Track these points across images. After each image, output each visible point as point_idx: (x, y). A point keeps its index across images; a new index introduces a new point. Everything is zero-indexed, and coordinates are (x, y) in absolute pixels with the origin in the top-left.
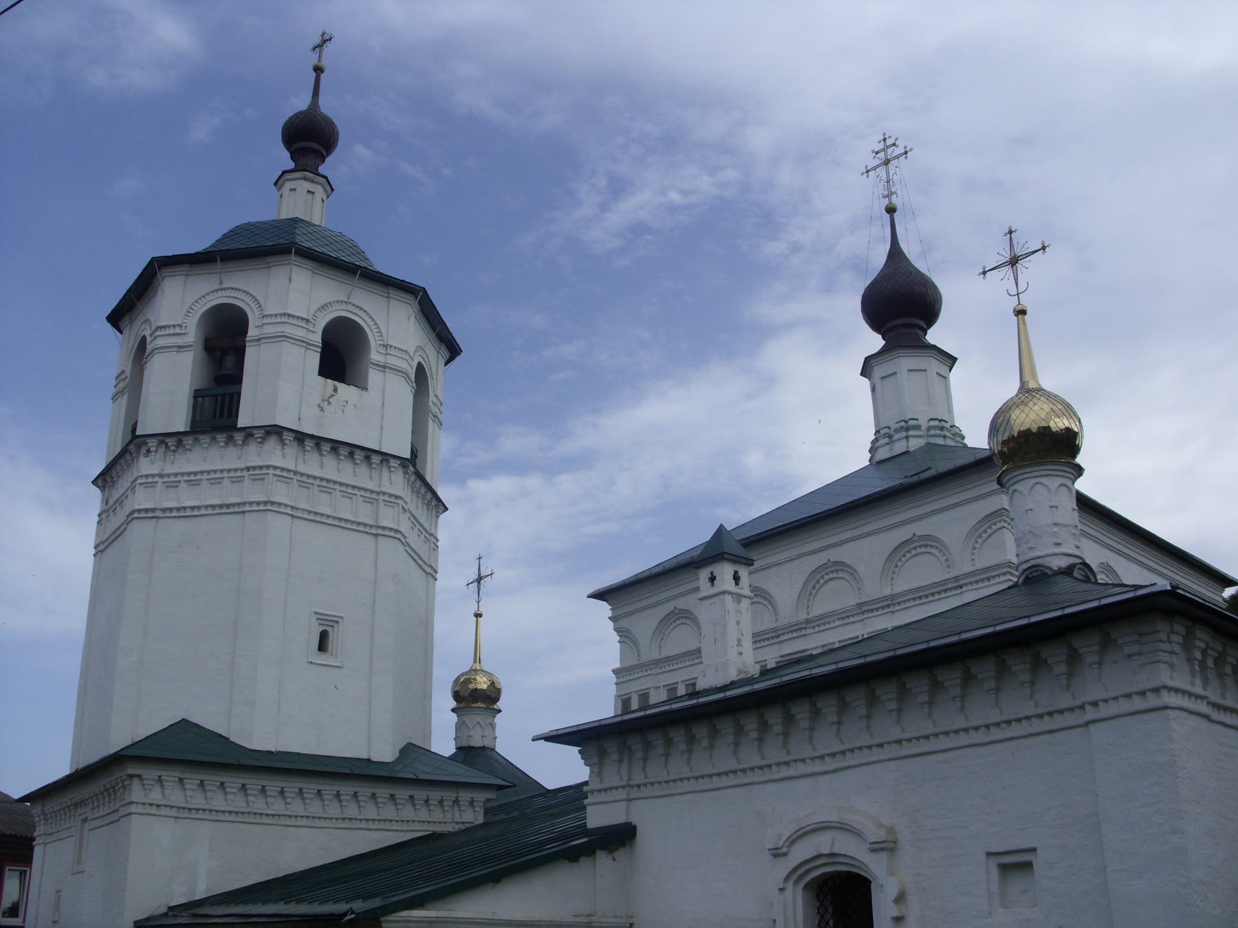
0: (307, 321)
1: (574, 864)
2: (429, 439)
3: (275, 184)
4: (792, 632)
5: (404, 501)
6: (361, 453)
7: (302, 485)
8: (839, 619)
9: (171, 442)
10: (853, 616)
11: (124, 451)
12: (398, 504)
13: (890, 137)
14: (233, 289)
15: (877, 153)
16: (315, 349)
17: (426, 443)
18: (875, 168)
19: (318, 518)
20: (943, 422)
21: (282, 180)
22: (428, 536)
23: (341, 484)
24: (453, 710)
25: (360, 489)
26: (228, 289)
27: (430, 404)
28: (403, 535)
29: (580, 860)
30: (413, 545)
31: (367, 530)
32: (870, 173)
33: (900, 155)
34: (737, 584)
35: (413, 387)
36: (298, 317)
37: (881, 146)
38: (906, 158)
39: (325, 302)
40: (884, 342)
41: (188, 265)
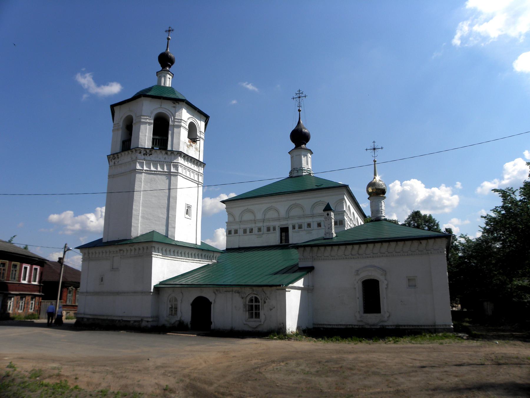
7: (193, 173)
9: (199, 163)
13: (301, 91)
14: (164, 108)
15: (297, 94)
18: (296, 98)
19: (187, 178)
33: (304, 96)
37: (298, 92)
38: (305, 98)
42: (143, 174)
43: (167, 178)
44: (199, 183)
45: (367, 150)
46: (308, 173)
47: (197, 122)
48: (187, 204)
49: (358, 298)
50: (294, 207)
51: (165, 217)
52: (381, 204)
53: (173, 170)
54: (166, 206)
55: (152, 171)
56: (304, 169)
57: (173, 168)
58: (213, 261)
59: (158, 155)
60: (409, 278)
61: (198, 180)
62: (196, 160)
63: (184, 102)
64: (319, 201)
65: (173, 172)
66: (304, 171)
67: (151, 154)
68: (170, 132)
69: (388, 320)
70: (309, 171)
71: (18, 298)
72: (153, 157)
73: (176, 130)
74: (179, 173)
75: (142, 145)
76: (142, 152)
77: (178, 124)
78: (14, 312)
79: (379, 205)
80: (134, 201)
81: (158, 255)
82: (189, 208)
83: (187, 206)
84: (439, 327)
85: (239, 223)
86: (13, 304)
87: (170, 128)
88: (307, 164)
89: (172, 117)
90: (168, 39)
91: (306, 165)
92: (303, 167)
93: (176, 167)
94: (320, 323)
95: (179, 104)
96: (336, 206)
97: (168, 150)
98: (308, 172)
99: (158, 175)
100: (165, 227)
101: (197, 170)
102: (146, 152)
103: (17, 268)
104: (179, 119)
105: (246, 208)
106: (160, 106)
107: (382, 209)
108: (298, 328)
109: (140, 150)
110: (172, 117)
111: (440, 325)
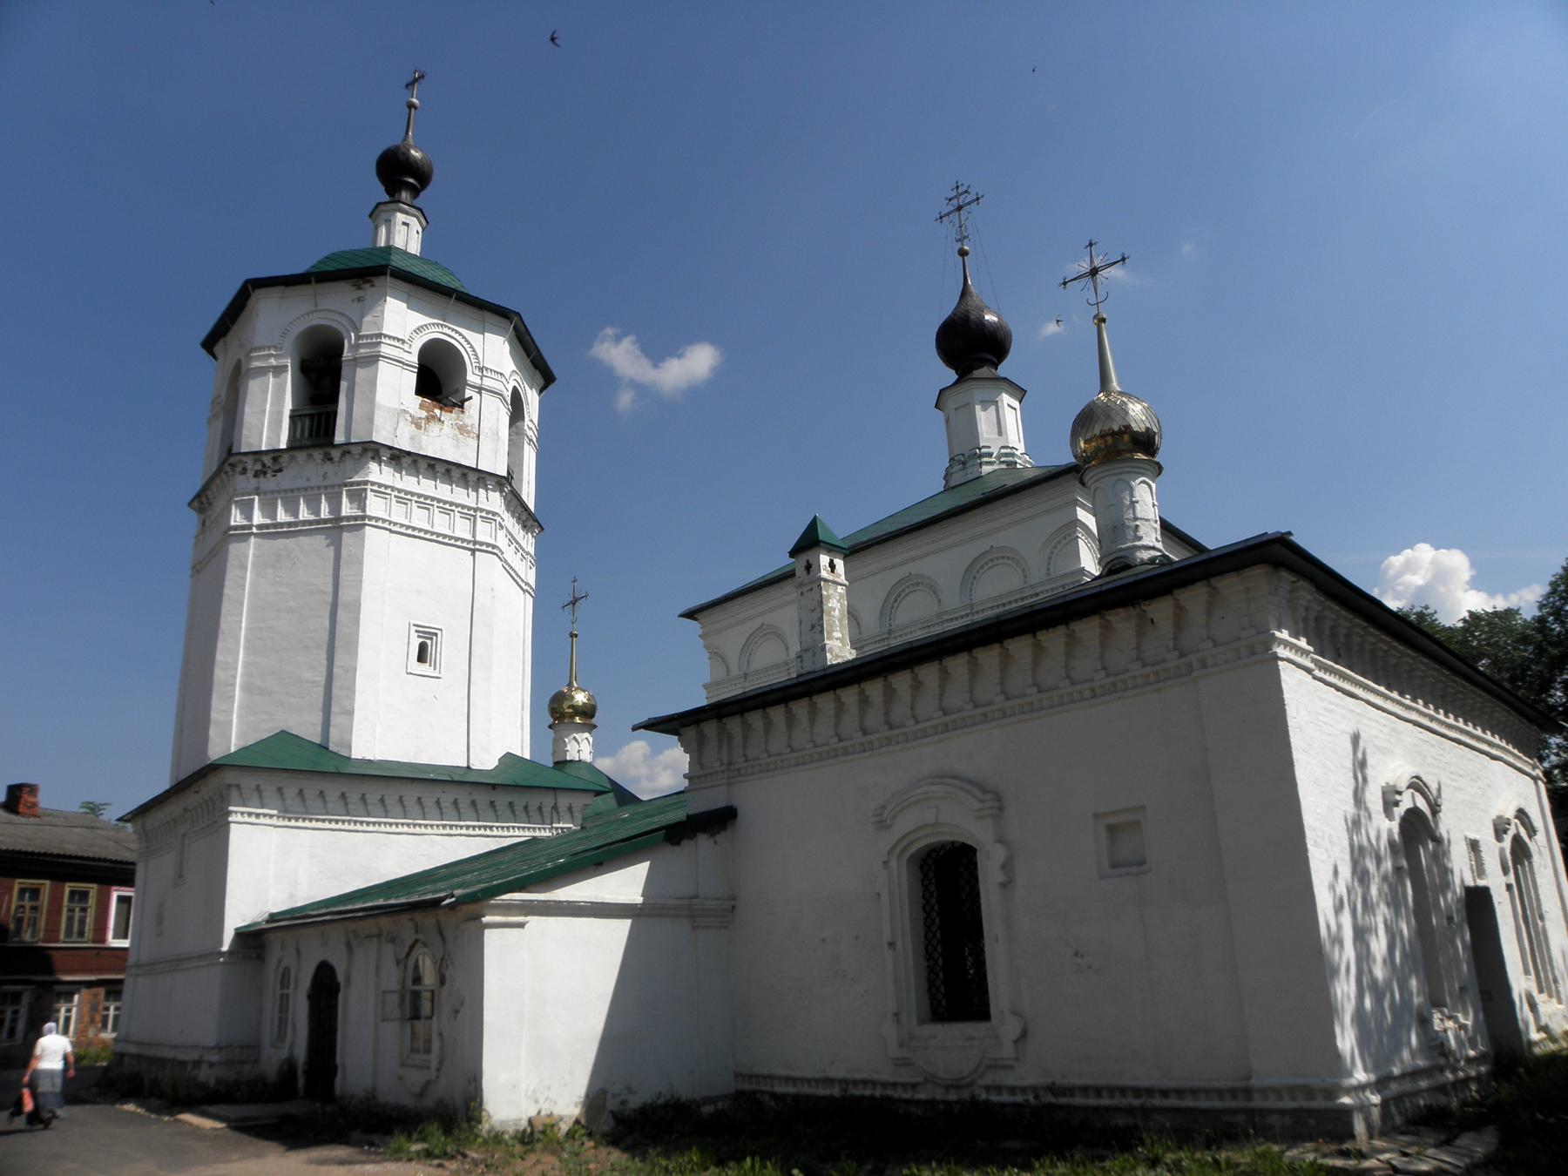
0: (403, 342)
1: (676, 847)
2: (524, 468)
3: (370, 216)
4: (875, 642)
5: (502, 518)
6: (457, 471)
7: (400, 500)
8: (920, 629)
10: (933, 625)
11: (220, 470)
12: (495, 520)
13: (962, 185)
14: (328, 310)
15: (950, 200)
16: (413, 369)
17: (522, 465)
18: (948, 214)
19: (416, 533)
20: (1014, 450)
21: (376, 212)
22: (525, 555)
23: (439, 501)
24: (550, 727)
25: (457, 505)
26: (324, 310)
27: (526, 428)
28: (501, 551)
29: (682, 843)
30: (510, 562)
31: (465, 545)
32: (944, 219)
34: (833, 571)
35: (509, 409)
36: (394, 338)
37: (954, 193)
39: (417, 325)
40: (957, 377)
41: (282, 287)
42: (252, 539)
43: (328, 541)
44: (477, 547)
45: (1065, 283)
46: (1003, 462)
47: (464, 337)
48: (414, 625)
49: (892, 945)
50: (907, 591)
51: (321, 678)
52: (1132, 495)
53: (347, 509)
54: (325, 637)
55: (282, 525)
56: (983, 450)
57: (351, 503)
58: (554, 825)
59: (309, 468)
60: (1112, 820)
61: (474, 536)
62: (454, 468)
63: (385, 274)
64: (988, 548)
65: (348, 518)
66: (985, 459)
67: (280, 470)
68: (344, 385)
69: (1017, 1059)
70: (1006, 455)
71: (96, 996)
72: (285, 480)
73: (361, 374)
74: (371, 518)
75: (250, 444)
76: (249, 466)
77: (368, 350)
78: (83, 1038)
79: (1121, 500)
80: (221, 637)
81: (258, 815)
82: (431, 639)
83: (416, 631)
84: (1272, 1103)
85: (743, 680)
86: (77, 1013)
87: (345, 371)
88: (1000, 433)
89: (352, 334)
90: (963, 253)
91: (996, 436)
92: (981, 445)
93: (359, 498)
94: (758, 1070)
95: (373, 286)
96: (1050, 558)
97: (335, 443)
98: (1002, 459)
99: (301, 535)
100: (321, 714)
101: (471, 502)
102: (264, 465)
103: (90, 901)
104: (371, 336)
105: (757, 623)
106: (313, 308)
107: (1136, 519)
108: (594, 1102)
109: (241, 461)
110: (352, 334)
111: (1277, 1092)
